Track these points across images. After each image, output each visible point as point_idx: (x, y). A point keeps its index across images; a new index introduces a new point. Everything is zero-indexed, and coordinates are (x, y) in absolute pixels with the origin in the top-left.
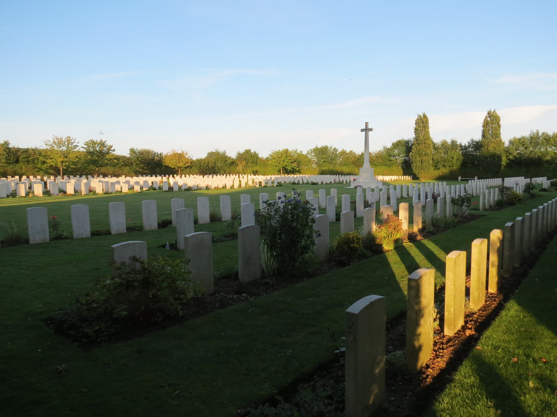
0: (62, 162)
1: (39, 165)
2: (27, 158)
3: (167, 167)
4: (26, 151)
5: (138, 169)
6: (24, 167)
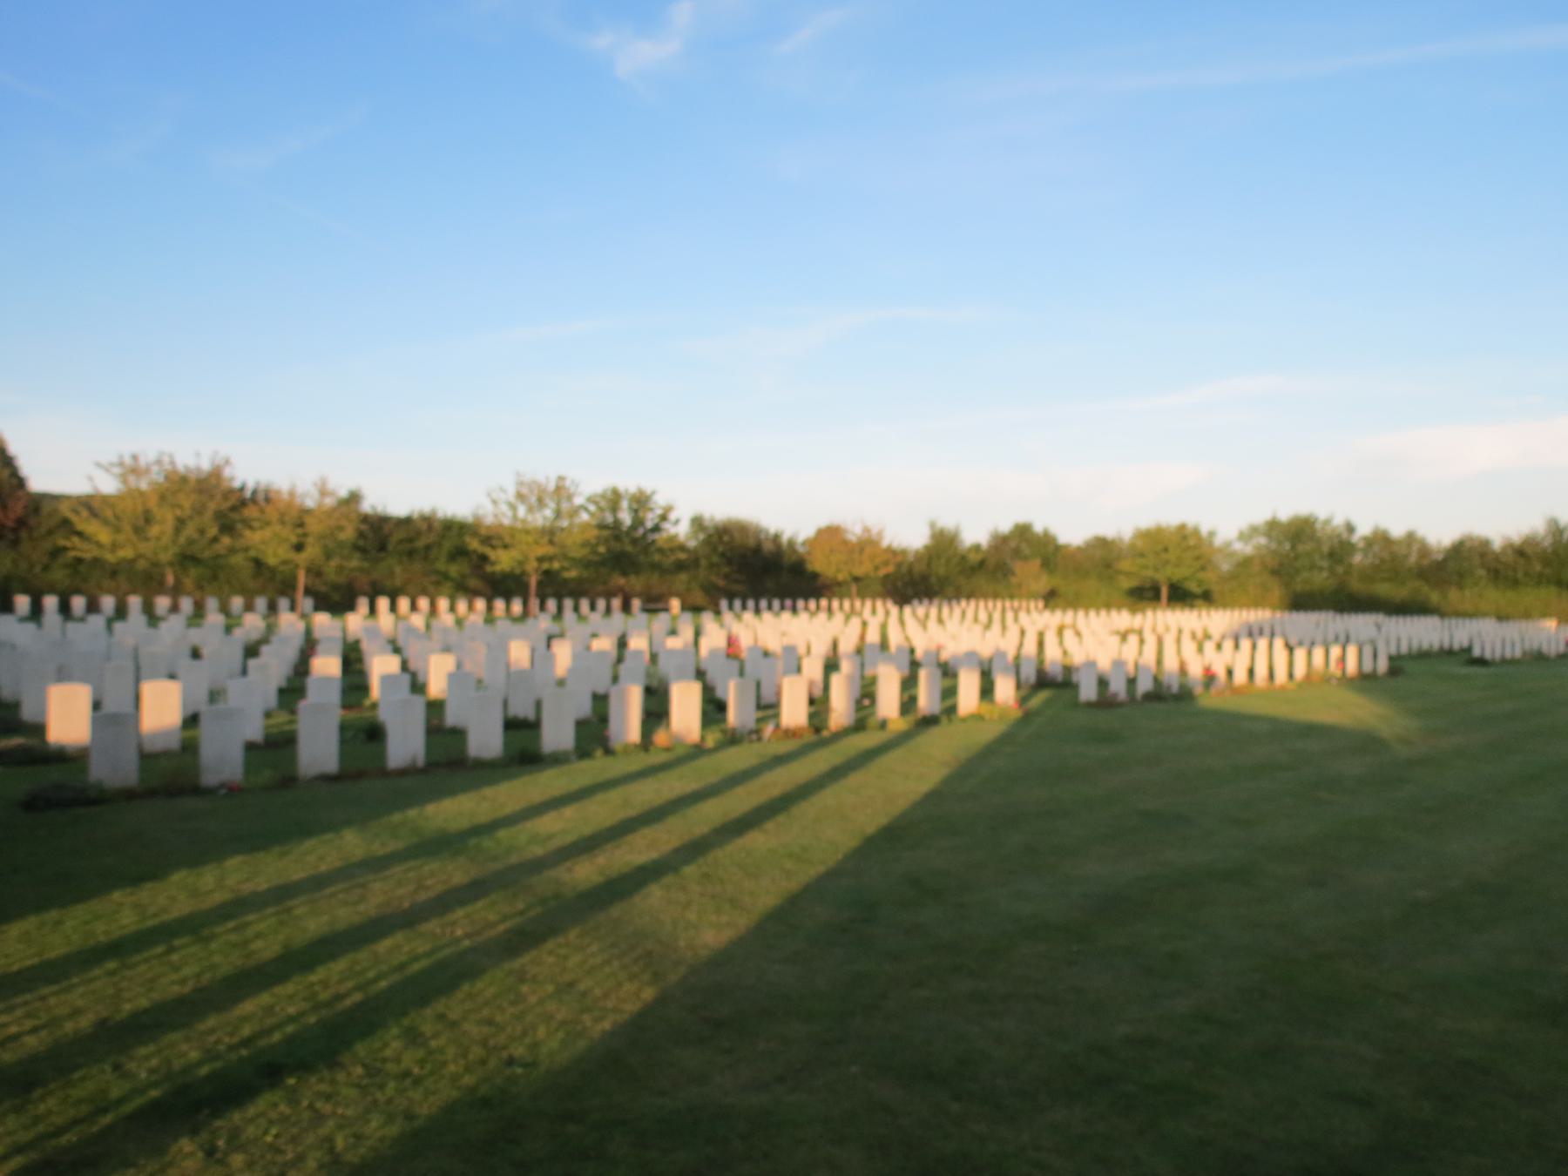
0: (541, 560)
1: (441, 565)
2: (411, 540)
3: (815, 576)
4: (407, 522)
5: (714, 578)
6: (398, 570)
